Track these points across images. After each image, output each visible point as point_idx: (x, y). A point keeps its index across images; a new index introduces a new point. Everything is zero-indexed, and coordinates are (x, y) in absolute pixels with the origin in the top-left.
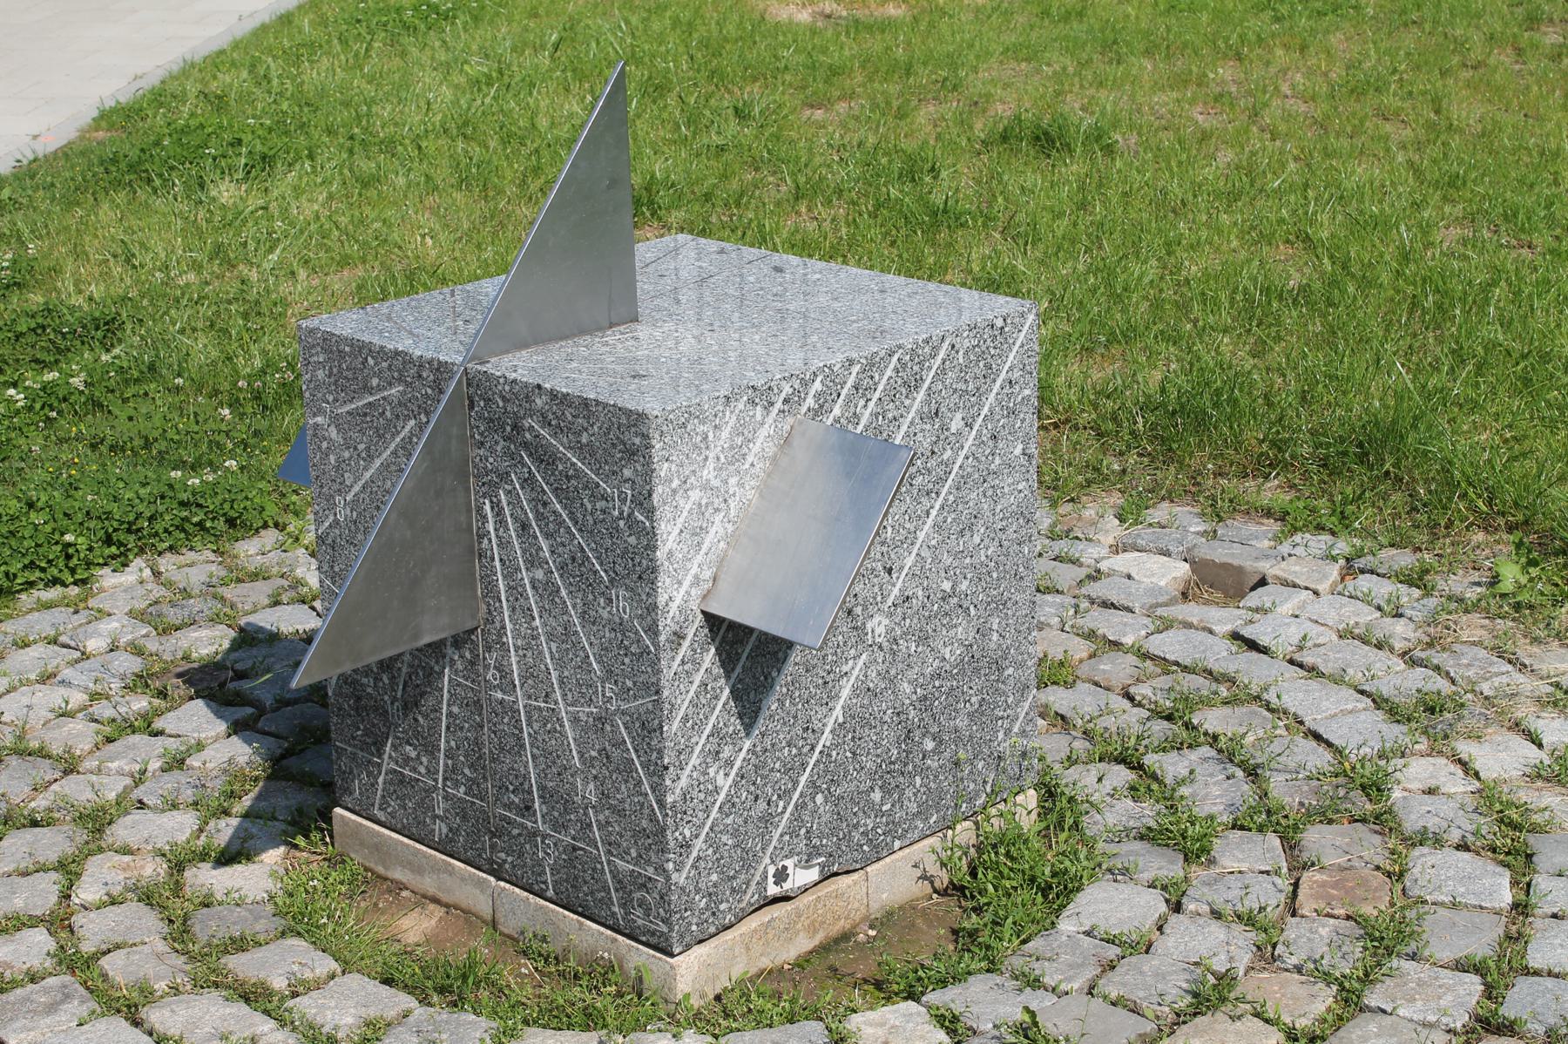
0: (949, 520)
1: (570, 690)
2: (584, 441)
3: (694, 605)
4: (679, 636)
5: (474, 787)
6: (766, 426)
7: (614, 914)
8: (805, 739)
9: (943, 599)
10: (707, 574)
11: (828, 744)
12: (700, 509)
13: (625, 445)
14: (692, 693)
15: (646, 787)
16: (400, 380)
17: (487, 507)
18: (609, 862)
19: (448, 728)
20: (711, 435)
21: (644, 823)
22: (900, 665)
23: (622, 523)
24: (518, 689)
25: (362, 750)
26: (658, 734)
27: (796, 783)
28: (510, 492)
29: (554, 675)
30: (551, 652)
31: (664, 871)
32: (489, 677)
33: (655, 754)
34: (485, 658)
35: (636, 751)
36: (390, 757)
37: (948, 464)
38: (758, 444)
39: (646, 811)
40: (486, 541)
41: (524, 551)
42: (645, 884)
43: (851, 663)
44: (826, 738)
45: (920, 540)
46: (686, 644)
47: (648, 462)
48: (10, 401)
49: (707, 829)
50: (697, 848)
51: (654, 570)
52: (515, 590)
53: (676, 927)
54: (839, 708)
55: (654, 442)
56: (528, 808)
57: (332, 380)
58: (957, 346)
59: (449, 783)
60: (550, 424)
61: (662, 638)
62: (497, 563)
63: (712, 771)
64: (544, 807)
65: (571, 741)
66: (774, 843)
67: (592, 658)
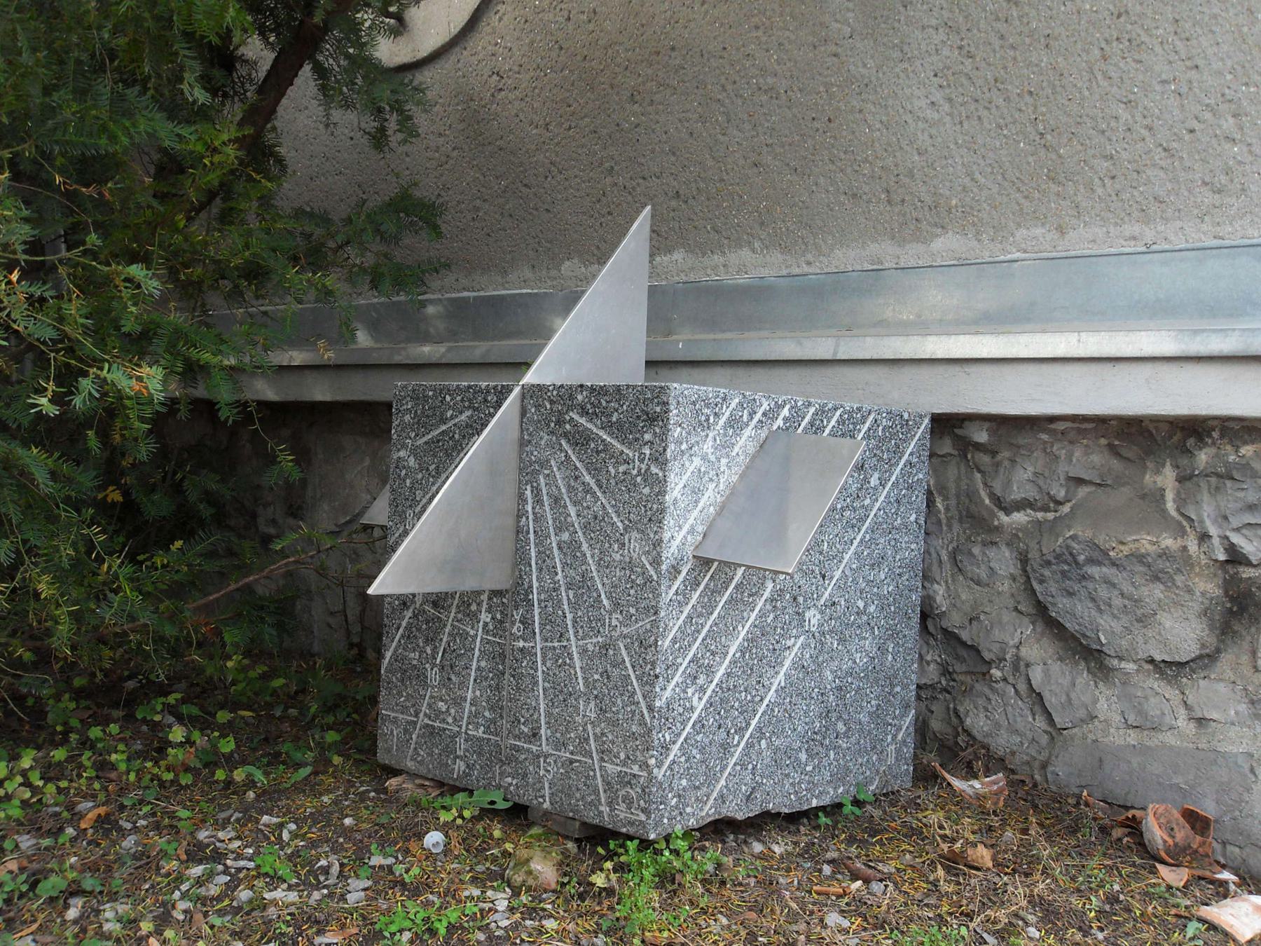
0: (865, 553)
1: (582, 627)
2: (614, 419)
3: (689, 551)
4: (675, 570)
5: (492, 726)
6: (750, 428)
7: (601, 813)
8: (757, 690)
9: (858, 613)
10: (700, 529)
11: (773, 701)
12: (699, 474)
13: (648, 415)
14: (680, 621)
15: (639, 697)
16: (469, 407)
17: (528, 493)
18: (601, 767)
19: (475, 680)
20: (712, 418)
21: (634, 728)
22: (826, 656)
23: (639, 479)
24: (538, 634)
25: (402, 713)
26: (653, 649)
27: (748, 724)
28: (548, 475)
29: (569, 617)
30: (569, 599)
31: (648, 766)
32: (515, 630)
33: (649, 666)
34: (513, 616)
35: (633, 667)
36: (425, 714)
37: (867, 509)
38: (743, 439)
39: (637, 717)
40: (524, 519)
41: (554, 520)
42: (627, 780)
43: (793, 639)
44: (771, 696)
45: (845, 561)
46: (681, 578)
47: (665, 430)
48: (224, 8)
49: (682, 739)
50: (674, 753)
51: (662, 511)
52: (544, 555)
53: (653, 816)
54: (782, 673)
55: (672, 407)
56: (535, 735)
57: (416, 420)
58: (879, 422)
59: (470, 727)
60: (587, 413)
61: (664, 567)
62: (532, 536)
63: (690, 691)
64: (549, 731)
65: (578, 670)
66: (729, 769)
67: (603, 596)
